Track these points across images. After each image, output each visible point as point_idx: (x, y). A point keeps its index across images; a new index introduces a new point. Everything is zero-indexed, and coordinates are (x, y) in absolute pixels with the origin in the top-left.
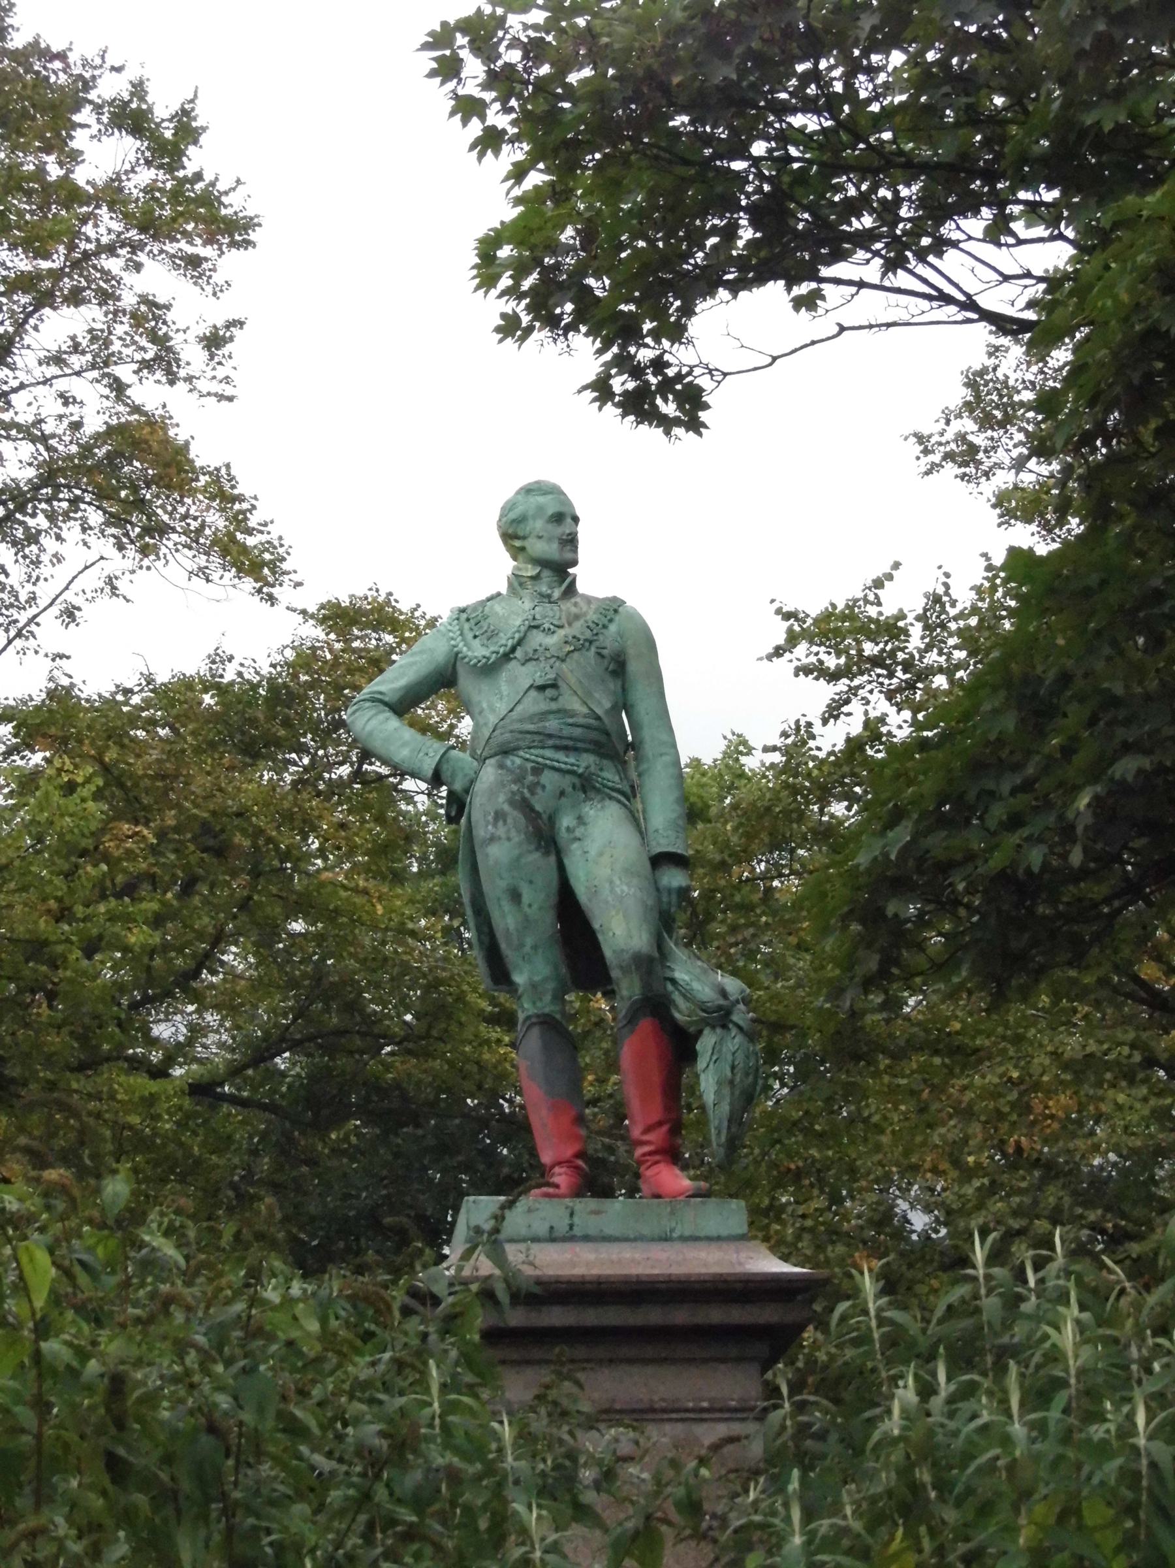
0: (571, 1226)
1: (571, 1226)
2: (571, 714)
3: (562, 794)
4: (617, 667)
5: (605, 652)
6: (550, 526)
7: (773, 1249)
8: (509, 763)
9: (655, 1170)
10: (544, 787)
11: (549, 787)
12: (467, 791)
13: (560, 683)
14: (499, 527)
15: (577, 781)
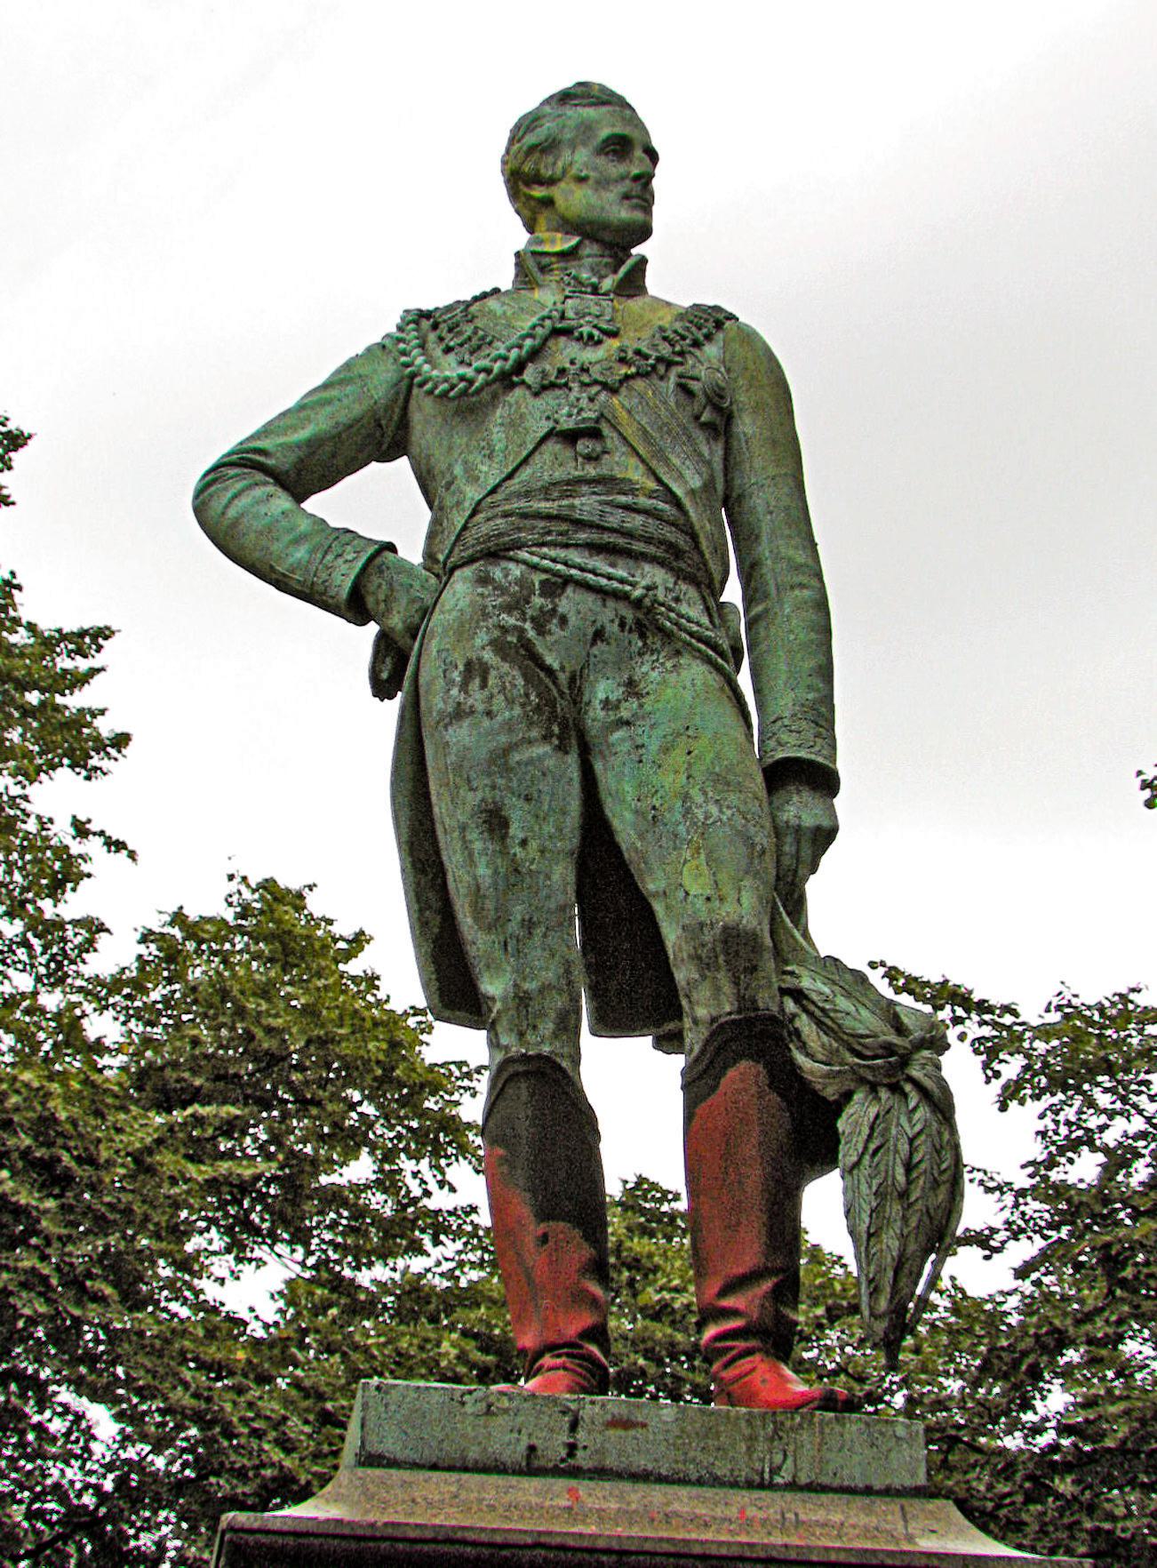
0: (572, 1448)
1: (572, 1448)
2: (628, 488)
3: (599, 635)
4: (718, 418)
5: (695, 386)
6: (601, 161)
7: (984, 1528)
8: (497, 574)
9: (744, 1364)
10: (563, 621)
11: (573, 620)
12: (413, 632)
13: (606, 430)
14: (504, 163)
15: (629, 615)
